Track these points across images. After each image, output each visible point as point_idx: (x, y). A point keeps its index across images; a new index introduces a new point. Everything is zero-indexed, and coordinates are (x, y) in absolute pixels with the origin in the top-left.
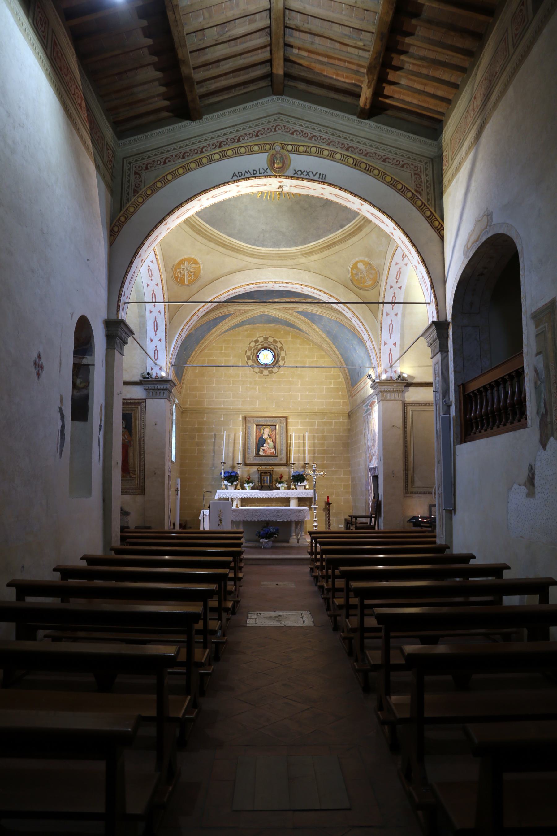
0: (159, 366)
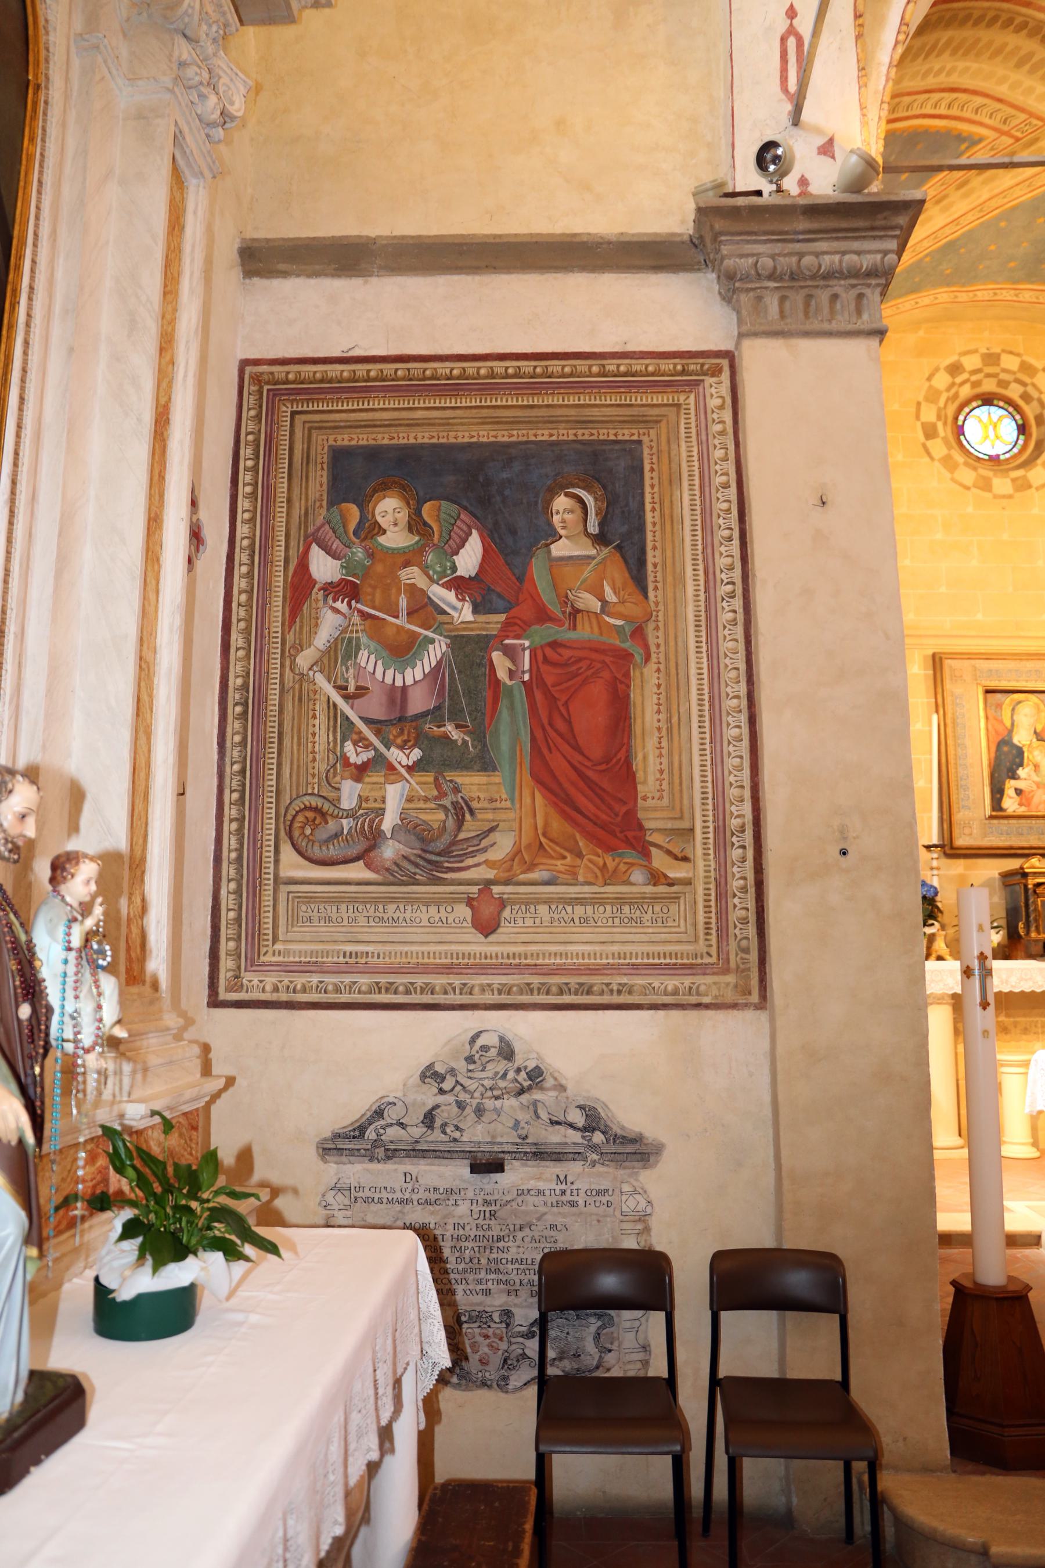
0: (818, 131)
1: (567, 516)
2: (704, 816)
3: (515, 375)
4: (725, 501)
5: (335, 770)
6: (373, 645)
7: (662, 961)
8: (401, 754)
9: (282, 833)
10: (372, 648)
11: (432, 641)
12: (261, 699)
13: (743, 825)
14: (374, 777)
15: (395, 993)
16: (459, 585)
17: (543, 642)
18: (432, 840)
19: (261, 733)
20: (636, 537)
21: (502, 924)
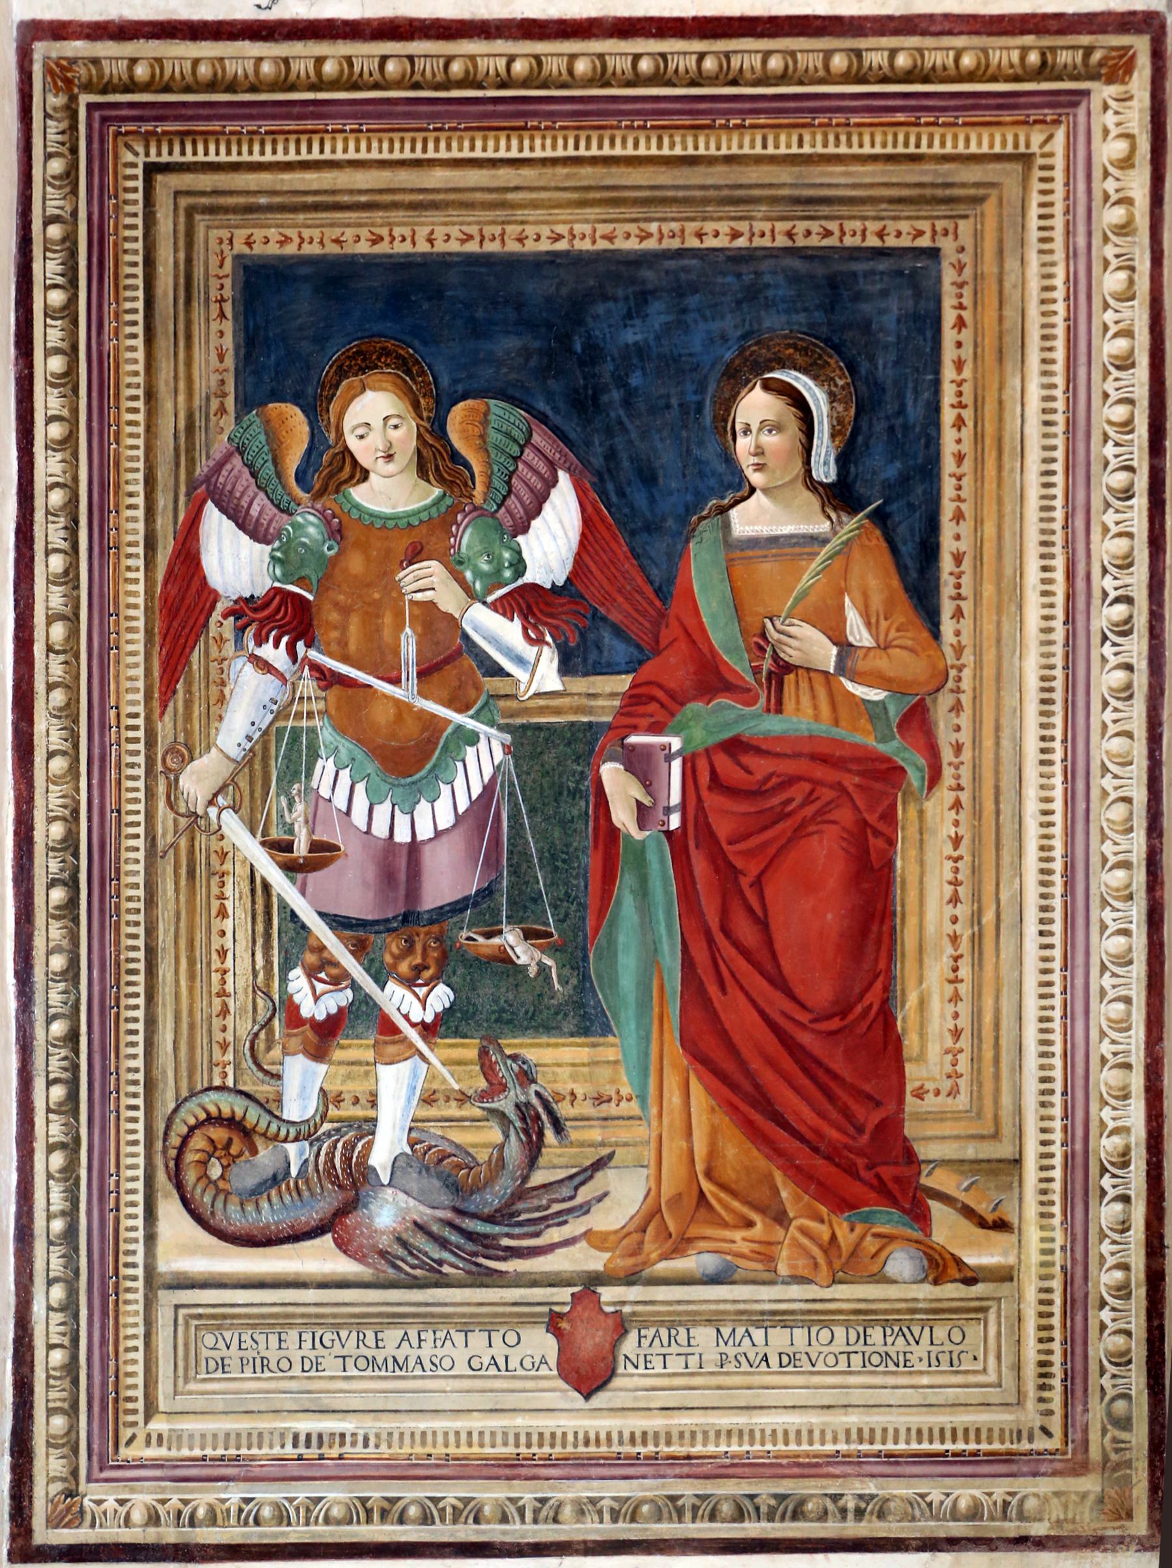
1: (770, 440)
2: (1044, 1130)
3: (656, 79)
4: (1120, 401)
5: (270, 1033)
6: (346, 747)
7: (949, 1446)
8: (409, 996)
9: (161, 1176)
10: (344, 754)
11: (473, 739)
12: (106, 874)
13: (1126, 1152)
14: (354, 1049)
15: (401, 1521)
16: (529, 604)
17: (711, 741)
18: (476, 1189)
19: (110, 950)
20: (919, 490)
21: (621, 1370)
